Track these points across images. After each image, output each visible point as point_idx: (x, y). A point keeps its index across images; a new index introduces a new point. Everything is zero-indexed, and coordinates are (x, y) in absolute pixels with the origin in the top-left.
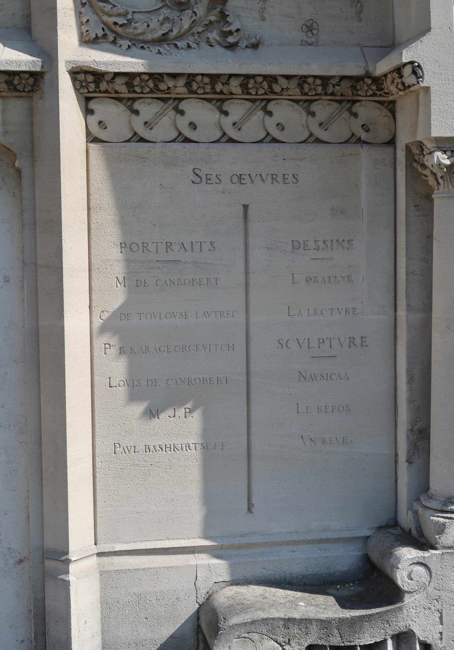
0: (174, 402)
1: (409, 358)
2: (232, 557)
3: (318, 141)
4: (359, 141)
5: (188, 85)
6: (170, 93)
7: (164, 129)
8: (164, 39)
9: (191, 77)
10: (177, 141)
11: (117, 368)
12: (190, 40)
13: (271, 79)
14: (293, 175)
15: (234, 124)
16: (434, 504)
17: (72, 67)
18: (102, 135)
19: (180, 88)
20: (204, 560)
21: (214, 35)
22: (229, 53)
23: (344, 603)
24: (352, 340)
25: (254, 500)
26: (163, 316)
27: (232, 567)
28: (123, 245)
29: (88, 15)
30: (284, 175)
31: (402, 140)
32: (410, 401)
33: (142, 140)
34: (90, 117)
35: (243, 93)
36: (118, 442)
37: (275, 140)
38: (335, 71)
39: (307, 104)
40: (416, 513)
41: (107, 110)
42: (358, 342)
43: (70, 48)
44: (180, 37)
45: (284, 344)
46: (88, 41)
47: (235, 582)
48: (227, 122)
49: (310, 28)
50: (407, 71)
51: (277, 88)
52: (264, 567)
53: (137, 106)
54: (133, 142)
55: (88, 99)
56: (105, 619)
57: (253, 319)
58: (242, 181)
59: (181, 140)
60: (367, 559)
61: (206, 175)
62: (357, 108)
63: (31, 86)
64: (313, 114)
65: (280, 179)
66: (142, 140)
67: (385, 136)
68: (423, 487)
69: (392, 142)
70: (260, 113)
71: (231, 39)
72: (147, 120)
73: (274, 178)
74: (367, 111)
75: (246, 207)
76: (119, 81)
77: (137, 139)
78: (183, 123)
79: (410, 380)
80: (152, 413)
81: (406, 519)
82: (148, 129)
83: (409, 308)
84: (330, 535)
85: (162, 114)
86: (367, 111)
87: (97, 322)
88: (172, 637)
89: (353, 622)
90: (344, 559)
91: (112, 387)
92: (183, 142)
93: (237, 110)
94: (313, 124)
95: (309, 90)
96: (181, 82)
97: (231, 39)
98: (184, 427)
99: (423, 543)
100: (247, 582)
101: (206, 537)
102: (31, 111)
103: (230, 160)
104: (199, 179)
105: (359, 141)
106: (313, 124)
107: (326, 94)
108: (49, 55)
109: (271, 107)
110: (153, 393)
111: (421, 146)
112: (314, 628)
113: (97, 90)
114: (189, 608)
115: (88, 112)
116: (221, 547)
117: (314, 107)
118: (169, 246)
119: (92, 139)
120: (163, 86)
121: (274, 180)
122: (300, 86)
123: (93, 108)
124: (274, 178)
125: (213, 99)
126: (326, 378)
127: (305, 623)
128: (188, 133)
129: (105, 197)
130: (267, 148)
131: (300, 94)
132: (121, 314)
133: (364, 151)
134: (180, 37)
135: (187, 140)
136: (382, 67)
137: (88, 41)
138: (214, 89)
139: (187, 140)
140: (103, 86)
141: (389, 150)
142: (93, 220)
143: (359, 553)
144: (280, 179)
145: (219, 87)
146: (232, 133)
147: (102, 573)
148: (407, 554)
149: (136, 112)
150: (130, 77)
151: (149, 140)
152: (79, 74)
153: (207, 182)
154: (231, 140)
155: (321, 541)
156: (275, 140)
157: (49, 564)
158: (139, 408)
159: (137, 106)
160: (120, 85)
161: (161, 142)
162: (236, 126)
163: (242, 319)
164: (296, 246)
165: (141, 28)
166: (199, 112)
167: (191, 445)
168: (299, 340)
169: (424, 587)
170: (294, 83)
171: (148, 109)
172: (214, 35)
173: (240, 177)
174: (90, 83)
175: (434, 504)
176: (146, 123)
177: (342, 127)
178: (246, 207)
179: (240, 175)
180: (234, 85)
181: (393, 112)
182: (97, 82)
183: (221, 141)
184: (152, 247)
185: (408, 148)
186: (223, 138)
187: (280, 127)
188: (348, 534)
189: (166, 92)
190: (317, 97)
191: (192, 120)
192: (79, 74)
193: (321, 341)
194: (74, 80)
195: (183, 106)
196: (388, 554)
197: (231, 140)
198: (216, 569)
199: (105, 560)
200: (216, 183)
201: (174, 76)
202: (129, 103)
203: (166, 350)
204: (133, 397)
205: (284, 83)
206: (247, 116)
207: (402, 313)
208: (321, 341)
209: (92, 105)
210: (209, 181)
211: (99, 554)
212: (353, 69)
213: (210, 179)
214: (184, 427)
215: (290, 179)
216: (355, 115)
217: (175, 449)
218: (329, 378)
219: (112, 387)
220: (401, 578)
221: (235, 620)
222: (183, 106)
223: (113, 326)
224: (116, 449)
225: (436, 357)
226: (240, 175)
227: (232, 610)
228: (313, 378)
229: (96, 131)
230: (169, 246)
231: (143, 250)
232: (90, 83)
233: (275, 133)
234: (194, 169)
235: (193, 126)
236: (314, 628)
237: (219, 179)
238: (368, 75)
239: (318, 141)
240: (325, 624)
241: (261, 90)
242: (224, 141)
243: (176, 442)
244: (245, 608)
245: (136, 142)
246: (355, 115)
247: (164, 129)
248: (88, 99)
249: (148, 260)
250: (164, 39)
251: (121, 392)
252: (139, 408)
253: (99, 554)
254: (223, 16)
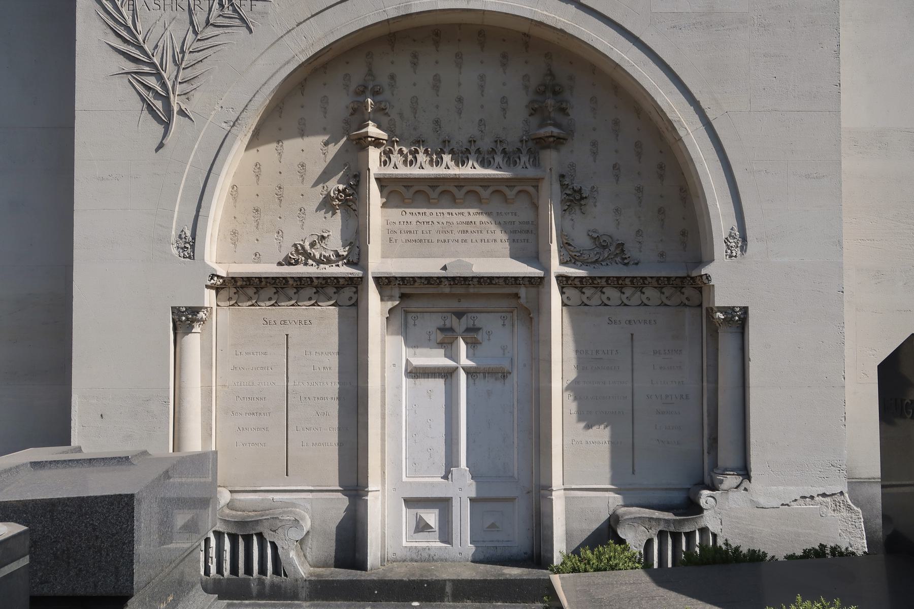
0: (599, 423)
1: (708, 405)
3: (666, 305)
4: (685, 305)
5: (607, 281)
7: (596, 300)
8: (596, 261)
9: (608, 278)
11: (573, 406)
12: (608, 262)
13: (644, 278)
16: (719, 471)
18: (568, 303)
19: (603, 282)
20: (340, 495)
21: (618, 259)
22: (625, 267)
23: (675, 515)
24: (682, 396)
25: (635, 468)
27: (624, 499)
28: (577, 351)
29: (564, 252)
32: (709, 425)
33: (586, 305)
37: (645, 305)
38: (673, 274)
39: (660, 288)
40: (711, 477)
41: (570, 292)
43: (556, 268)
44: (603, 261)
46: (562, 263)
47: (625, 506)
48: (624, 297)
49: (662, 255)
50: (704, 277)
51: (647, 282)
53: (584, 290)
55: (563, 288)
56: (567, 518)
57: (635, 385)
60: (689, 499)
62: (683, 290)
63: (538, 283)
64: (663, 293)
66: (586, 305)
67: (698, 303)
68: (715, 465)
69: (700, 305)
70: (639, 293)
71: (626, 261)
74: (689, 291)
75: (632, 335)
76: (577, 280)
78: (604, 297)
79: (709, 415)
80: (588, 427)
81: (707, 480)
83: (708, 381)
84: (671, 486)
86: (689, 291)
87: (565, 385)
88: (597, 529)
89: (680, 521)
90: (678, 497)
93: (628, 291)
94: (663, 298)
95: (661, 283)
96: (604, 280)
97: (626, 261)
98: (602, 435)
99: (713, 488)
100: (632, 506)
101: (612, 484)
102: (538, 294)
105: (685, 305)
106: (663, 298)
108: (547, 270)
109: (644, 290)
110: (589, 413)
111: (712, 309)
112: (662, 523)
114: (605, 517)
115: (562, 293)
116: (620, 489)
117: (664, 290)
118: (597, 352)
119: (564, 304)
120: (595, 282)
122: (657, 281)
127: (658, 520)
128: (607, 302)
129: (568, 330)
130: (642, 308)
132: (575, 381)
133: (687, 310)
134: (603, 261)
135: (606, 305)
136: (694, 274)
137: (562, 263)
138: (618, 283)
139: (606, 305)
140: (570, 282)
141: (699, 309)
145: (620, 282)
146: (626, 302)
147: (566, 498)
148: (705, 493)
149: (584, 293)
150: (581, 278)
152: (559, 278)
154: (625, 305)
155: (666, 489)
156: (645, 305)
157: (542, 492)
158: (583, 425)
159: (584, 290)
160: (577, 282)
163: (630, 385)
164: (655, 352)
165: (586, 257)
166: (612, 293)
169: (713, 507)
170: (654, 280)
171: (588, 292)
172: (618, 259)
173: (630, 321)
174: (564, 281)
175: (719, 471)
177: (637, 298)
178: (632, 335)
180: (627, 281)
181: (701, 292)
182: (567, 281)
185: (707, 309)
187: (648, 299)
188: (680, 487)
192: (559, 278)
193: (667, 396)
194: (557, 280)
195: (604, 290)
196: (698, 496)
197: (625, 305)
198: (614, 500)
199: (567, 492)
201: (601, 278)
202: (581, 289)
204: (580, 419)
205: (650, 280)
206: (633, 294)
207: (705, 384)
208: (667, 396)
209: (564, 290)
211: (565, 489)
212: (682, 274)
214: (602, 435)
220: (702, 502)
221: (627, 517)
222: (604, 290)
223: (573, 388)
225: (720, 404)
227: (625, 514)
229: (566, 301)
230: (597, 352)
232: (564, 281)
233: (646, 302)
235: (609, 299)
236: (662, 523)
238: (688, 276)
239: (666, 305)
240: (667, 521)
241: (639, 283)
244: (631, 513)
246: (683, 293)
247: (596, 300)
248: (563, 288)
249: (588, 357)
250: (596, 261)
251: (575, 416)
252: (583, 425)
253: (565, 489)
254: (623, 251)
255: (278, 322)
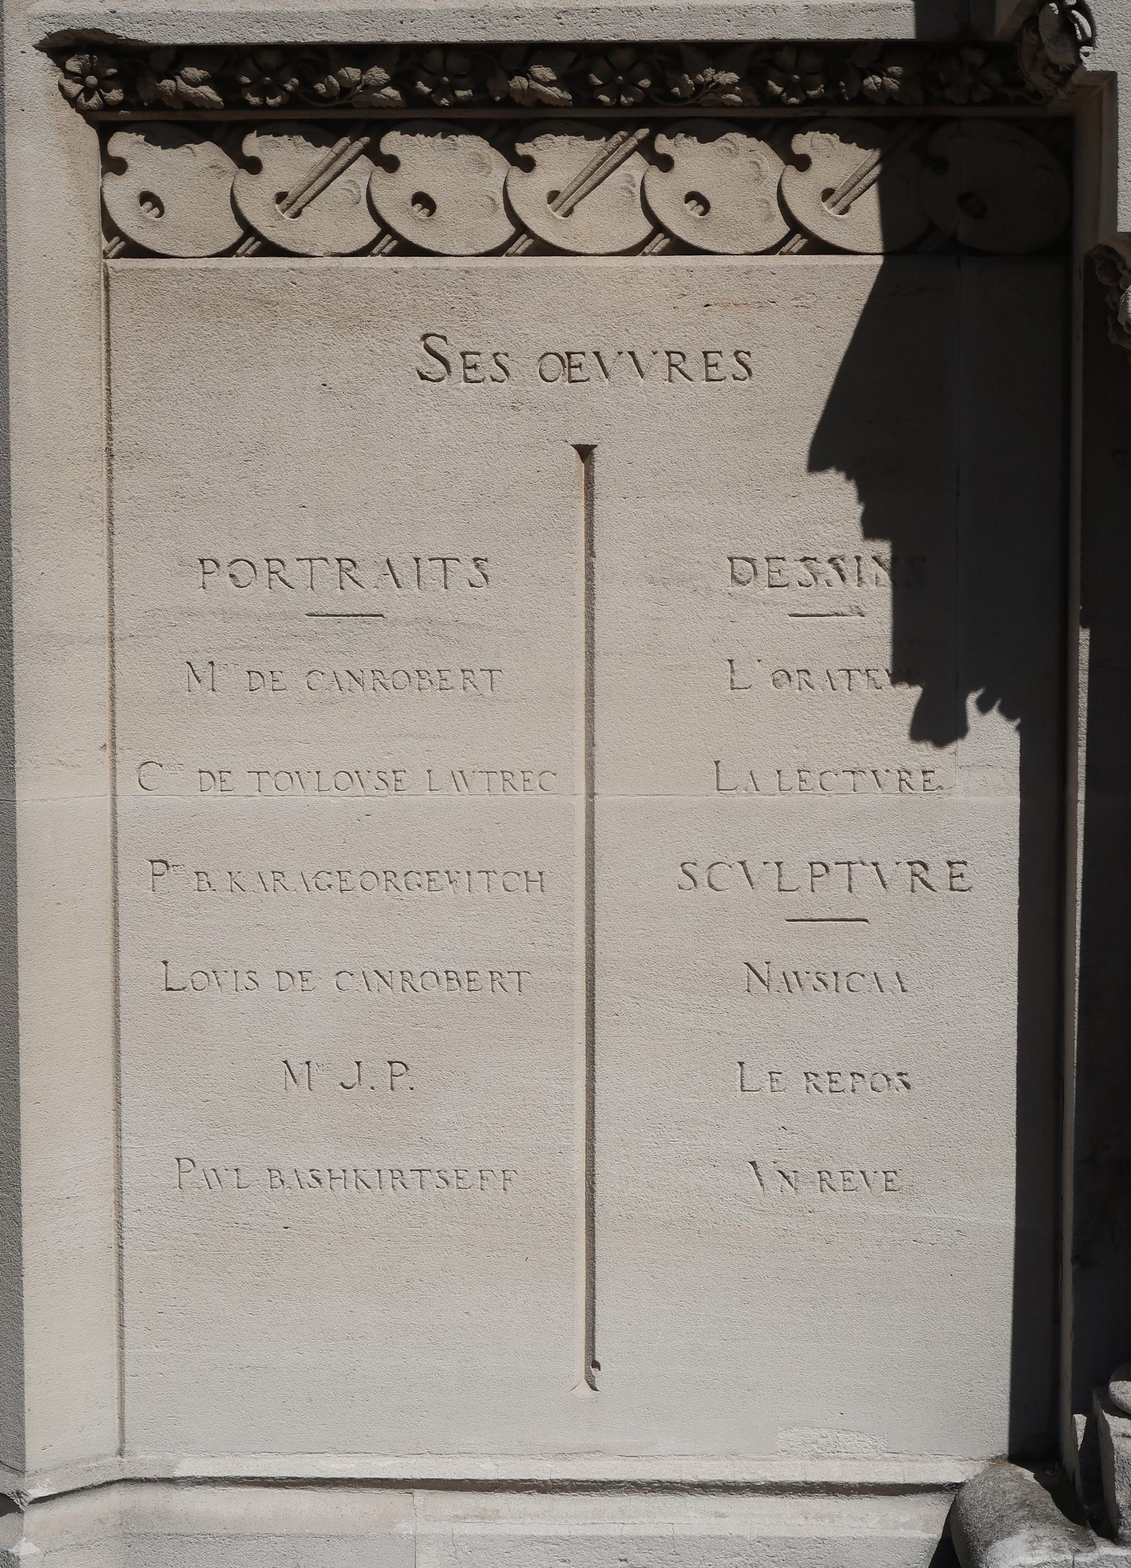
2: (529, 1520)
6: (349, 106)
10: (375, 251)
14: (737, 353)
15: (553, 196)
17: (49, 35)
26: (327, 780)
30: (705, 354)
31: (1084, 244)
34: (112, 180)
35: (577, 102)
36: (190, 1156)
42: (938, 875)
45: (702, 878)
48: (529, 193)
52: (622, 1556)
53: (801, 144)
54: (244, 254)
58: (576, 373)
59: (387, 250)
61: (463, 355)
65: (693, 365)
72: (830, 185)
73: (675, 360)
77: (254, 247)
82: (558, 215)
85: (332, 173)
91: (171, 989)
92: (394, 253)
103: (532, 306)
104: (440, 366)
107: (839, 100)
113: (132, 100)
121: (674, 369)
123: (122, 155)
124: (675, 360)
125: (490, 121)
126: (832, 986)
128: (409, 225)
131: (757, 103)
142: (119, 493)
143: (925, 1536)
144: (693, 365)
151: (291, 248)
153: (465, 375)
161: (326, 255)
162: (557, 202)
167: (409, 1175)
168: (747, 864)
171: (287, 159)
173: (567, 359)
176: (281, 197)
179: (569, 354)
183: (511, 250)
184: (295, 571)
186: (518, 242)
189: (690, 102)
190: (812, 112)
191: (150, 188)
200: (494, 380)
203: (426, 885)
208: (820, 868)
210: (471, 374)
213: (475, 367)
215: (728, 364)
216: (940, 165)
217: (361, 1184)
218: (843, 988)
219: (171, 989)
224: (184, 1176)
226: (569, 354)
228: (792, 981)
231: (270, 580)
234: (425, 337)
237: (745, 366)
242: (519, 251)
243: (360, 1164)
245: (253, 255)
246: (940, 165)
255: (523, 366)
